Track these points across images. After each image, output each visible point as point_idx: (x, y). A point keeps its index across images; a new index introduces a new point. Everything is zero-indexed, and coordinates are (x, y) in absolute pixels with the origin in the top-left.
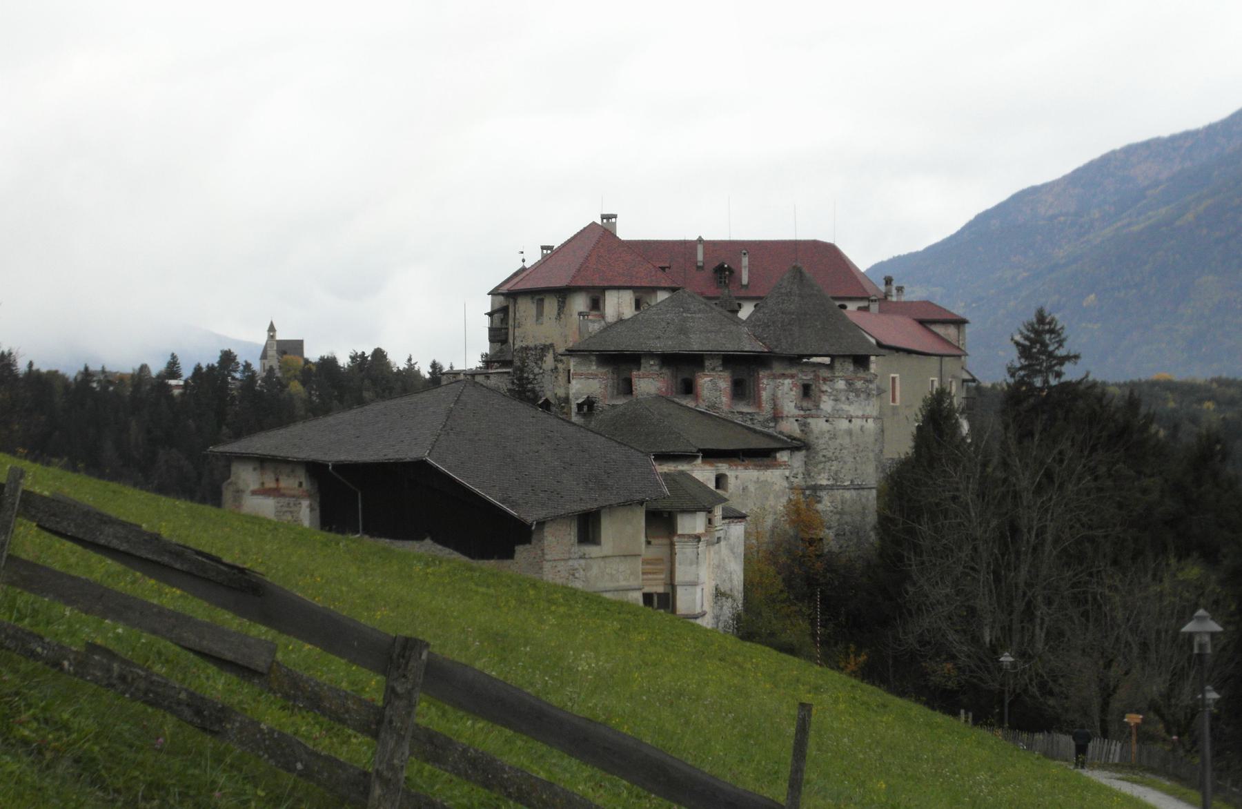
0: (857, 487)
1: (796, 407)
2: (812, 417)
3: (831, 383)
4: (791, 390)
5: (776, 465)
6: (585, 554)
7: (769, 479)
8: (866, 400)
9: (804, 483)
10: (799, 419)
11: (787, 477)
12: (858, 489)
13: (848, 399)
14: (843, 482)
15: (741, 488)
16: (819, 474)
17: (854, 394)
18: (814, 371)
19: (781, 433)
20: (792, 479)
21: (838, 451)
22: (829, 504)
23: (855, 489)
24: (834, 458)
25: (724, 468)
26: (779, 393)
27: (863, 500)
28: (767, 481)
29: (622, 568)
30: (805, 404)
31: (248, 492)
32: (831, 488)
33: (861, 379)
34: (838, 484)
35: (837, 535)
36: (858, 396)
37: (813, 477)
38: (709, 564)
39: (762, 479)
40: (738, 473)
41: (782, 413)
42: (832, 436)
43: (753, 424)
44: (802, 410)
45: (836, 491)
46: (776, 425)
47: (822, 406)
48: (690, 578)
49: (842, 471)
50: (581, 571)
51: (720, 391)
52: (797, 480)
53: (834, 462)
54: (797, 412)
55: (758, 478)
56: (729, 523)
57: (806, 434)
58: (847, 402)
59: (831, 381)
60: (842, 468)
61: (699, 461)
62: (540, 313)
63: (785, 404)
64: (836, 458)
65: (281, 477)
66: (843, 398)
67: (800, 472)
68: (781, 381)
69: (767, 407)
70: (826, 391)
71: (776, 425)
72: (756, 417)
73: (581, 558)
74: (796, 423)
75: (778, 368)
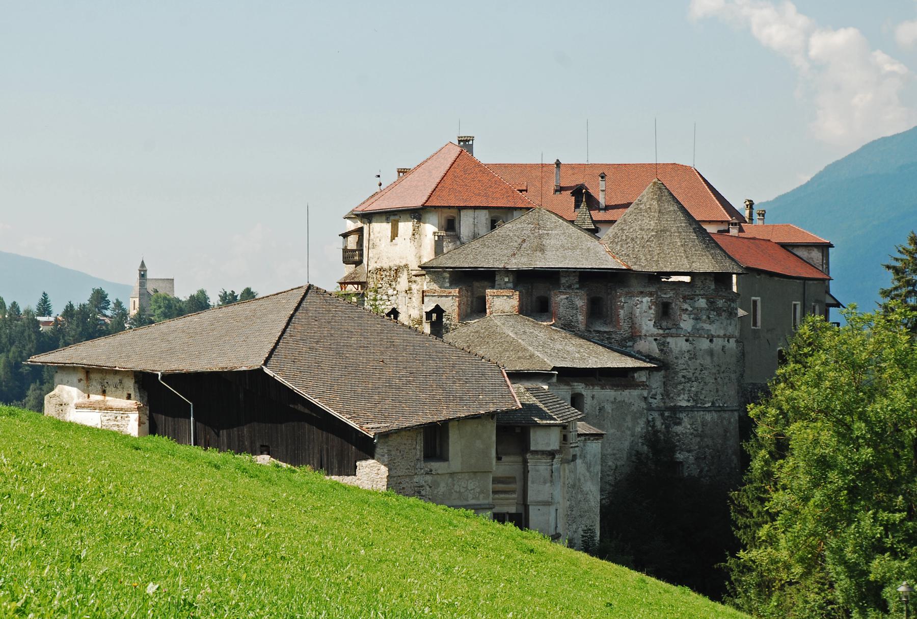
0: (720, 409)
2: (672, 336)
4: (650, 308)
5: (635, 385)
6: (431, 471)
7: (626, 399)
8: (728, 319)
9: (662, 404)
10: (658, 338)
11: (645, 398)
12: (719, 411)
13: (709, 318)
15: (598, 408)
16: (679, 395)
17: (715, 313)
18: (674, 289)
20: (651, 400)
21: (698, 372)
22: (689, 426)
23: (715, 411)
26: (637, 312)
27: (725, 423)
28: (624, 401)
29: (471, 486)
30: (664, 324)
31: (72, 405)
34: (699, 405)
35: (697, 459)
36: (719, 315)
37: (672, 398)
38: (564, 484)
39: (619, 399)
40: (594, 393)
41: (641, 332)
42: (692, 356)
43: (610, 343)
44: (661, 328)
45: (696, 412)
46: (634, 344)
47: (682, 325)
48: (544, 497)
49: (704, 392)
50: (428, 488)
51: (577, 309)
52: (655, 401)
54: (655, 331)
55: (615, 399)
56: (585, 440)
58: (708, 321)
59: (692, 299)
60: (702, 389)
62: (394, 234)
63: (643, 323)
64: (697, 379)
65: (107, 389)
66: (704, 317)
67: (658, 392)
69: (625, 326)
70: (687, 310)
73: (427, 473)
74: (654, 343)
75: (636, 286)
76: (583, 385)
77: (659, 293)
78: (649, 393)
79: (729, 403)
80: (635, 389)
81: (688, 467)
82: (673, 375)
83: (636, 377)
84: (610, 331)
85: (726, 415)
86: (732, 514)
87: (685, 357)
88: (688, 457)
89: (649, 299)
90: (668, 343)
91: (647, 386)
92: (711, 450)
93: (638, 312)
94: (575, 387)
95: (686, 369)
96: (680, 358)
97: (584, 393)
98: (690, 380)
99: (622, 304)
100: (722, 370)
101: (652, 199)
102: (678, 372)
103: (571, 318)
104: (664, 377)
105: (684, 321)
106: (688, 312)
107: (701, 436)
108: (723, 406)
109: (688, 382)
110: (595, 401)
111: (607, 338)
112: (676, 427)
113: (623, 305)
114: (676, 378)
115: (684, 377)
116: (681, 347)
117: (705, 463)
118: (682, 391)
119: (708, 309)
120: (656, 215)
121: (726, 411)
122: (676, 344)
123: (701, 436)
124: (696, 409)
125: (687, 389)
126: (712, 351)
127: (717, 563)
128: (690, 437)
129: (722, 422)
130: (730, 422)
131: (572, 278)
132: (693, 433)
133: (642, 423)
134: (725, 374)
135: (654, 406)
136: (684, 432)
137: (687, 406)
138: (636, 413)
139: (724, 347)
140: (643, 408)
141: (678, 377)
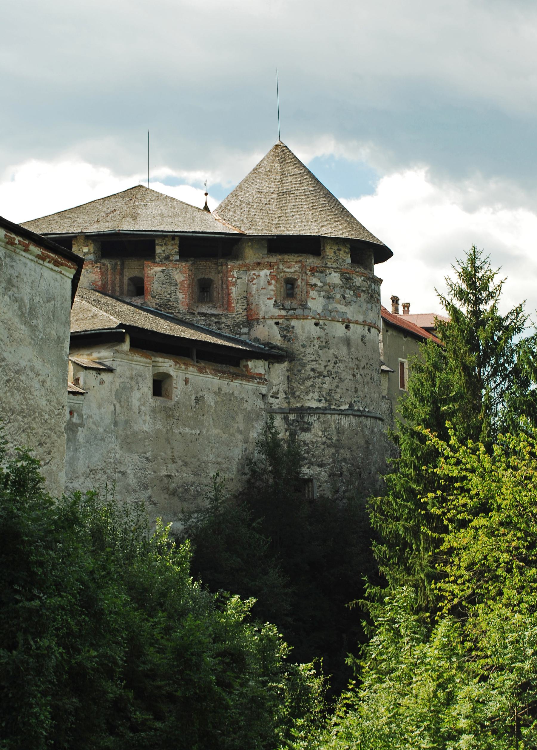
0: (359, 413)
1: (276, 305)
2: (297, 319)
3: (321, 275)
4: (269, 283)
5: (250, 377)
7: (236, 393)
8: (368, 302)
9: (286, 405)
11: (263, 396)
12: (359, 416)
13: (344, 298)
14: (339, 406)
15: (193, 397)
16: (307, 393)
17: (352, 293)
18: (300, 261)
19: (256, 340)
20: (271, 400)
21: (331, 364)
22: (320, 434)
23: (354, 415)
24: (325, 373)
25: (167, 365)
27: (367, 432)
28: (233, 394)
30: (287, 303)
32: (323, 411)
33: (362, 274)
36: (357, 295)
37: (299, 397)
40: (188, 376)
41: (258, 314)
42: (324, 344)
43: (219, 329)
44: (284, 309)
45: (329, 416)
46: (250, 330)
47: (310, 304)
49: (339, 390)
51: (176, 285)
52: (277, 401)
53: (327, 379)
54: (277, 312)
57: (289, 341)
58: (343, 301)
59: (322, 272)
60: (337, 387)
61: (126, 346)
63: (261, 302)
64: (330, 374)
66: (338, 296)
67: (281, 389)
68: (256, 272)
69: (238, 307)
70: (315, 285)
71: (250, 330)
72: (224, 320)
76: (172, 363)
77: (281, 267)
78: (268, 391)
79: (371, 408)
80: (249, 381)
81: (320, 486)
82: (300, 368)
83: (250, 367)
84: (219, 315)
85: (368, 422)
86: (372, 521)
87: (314, 346)
88: (320, 474)
89: (268, 272)
90: (293, 327)
91: (266, 380)
92: (349, 465)
93: (254, 289)
94: (160, 364)
95: (316, 361)
96: (308, 346)
97: (172, 373)
98: (320, 374)
99: (234, 279)
100: (362, 366)
101: (273, 161)
102: (305, 364)
103: (168, 296)
104: (288, 371)
105: (313, 299)
106: (317, 288)
107: (335, 446)
108: (364, 410)
109: (318, 377)
110: (189, 386)
111: (216, 323)
112: (303, 434)
113: (236, 282)
114: (303, 372)
115: (313, 370)
116: (309, 332)
117: (342, 481)
118: (310, 388)
119: (342, 287)
120: (278, 177)
121: (367, 417)
122: (303, 328)
123: (335, 446)
124: (329, 412)
125: (317, 386)
126: (349, 340)
127: (352, 600)
128: (322, 447)
129: (362, 430)
130: (372, 432)
131: (170, 247)
132: (325, 442)
133: (259, 426)
134: (366, 371)
135: (275, 407)
136: (314, 440)
137: (317, 408)
138: (250, 413)
139: (363, 336)
140: (260, 408)
141: (306, 371)
